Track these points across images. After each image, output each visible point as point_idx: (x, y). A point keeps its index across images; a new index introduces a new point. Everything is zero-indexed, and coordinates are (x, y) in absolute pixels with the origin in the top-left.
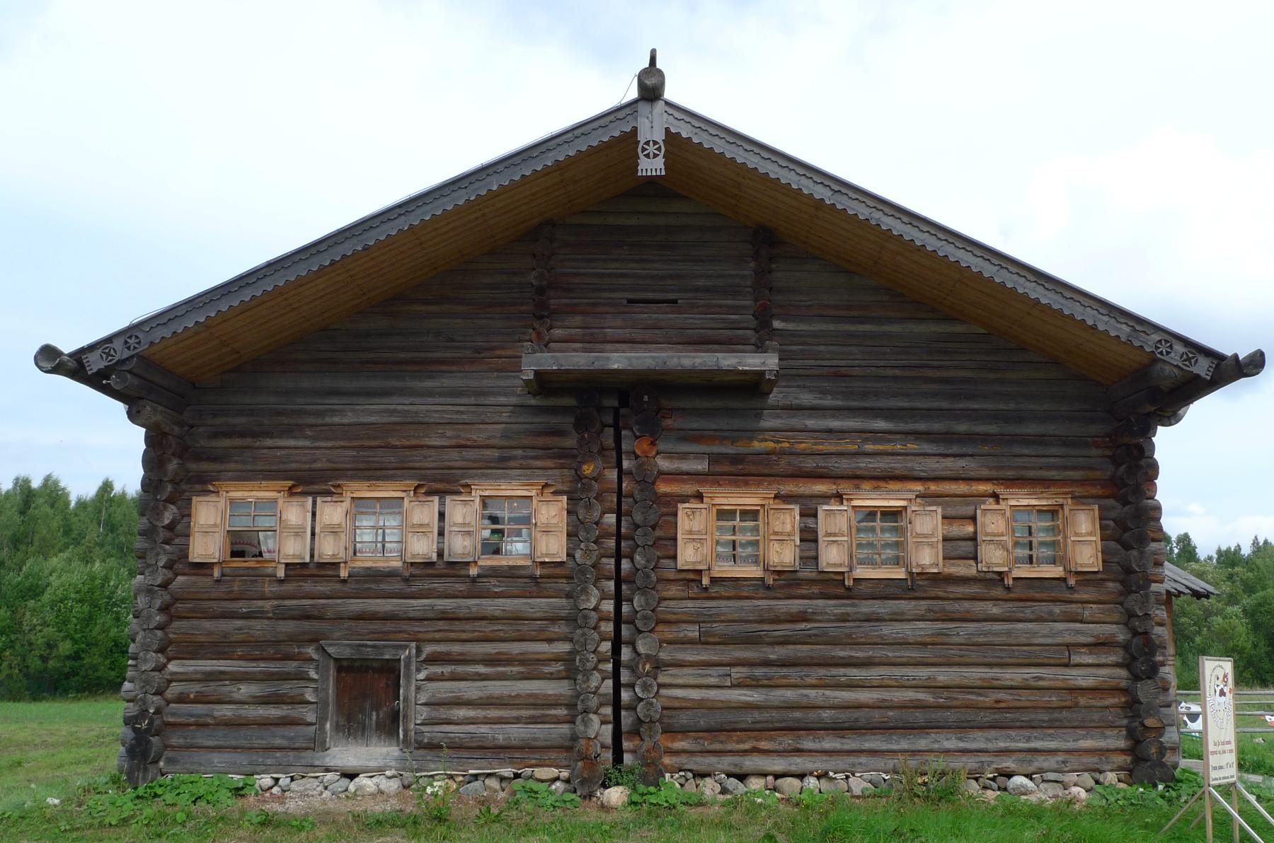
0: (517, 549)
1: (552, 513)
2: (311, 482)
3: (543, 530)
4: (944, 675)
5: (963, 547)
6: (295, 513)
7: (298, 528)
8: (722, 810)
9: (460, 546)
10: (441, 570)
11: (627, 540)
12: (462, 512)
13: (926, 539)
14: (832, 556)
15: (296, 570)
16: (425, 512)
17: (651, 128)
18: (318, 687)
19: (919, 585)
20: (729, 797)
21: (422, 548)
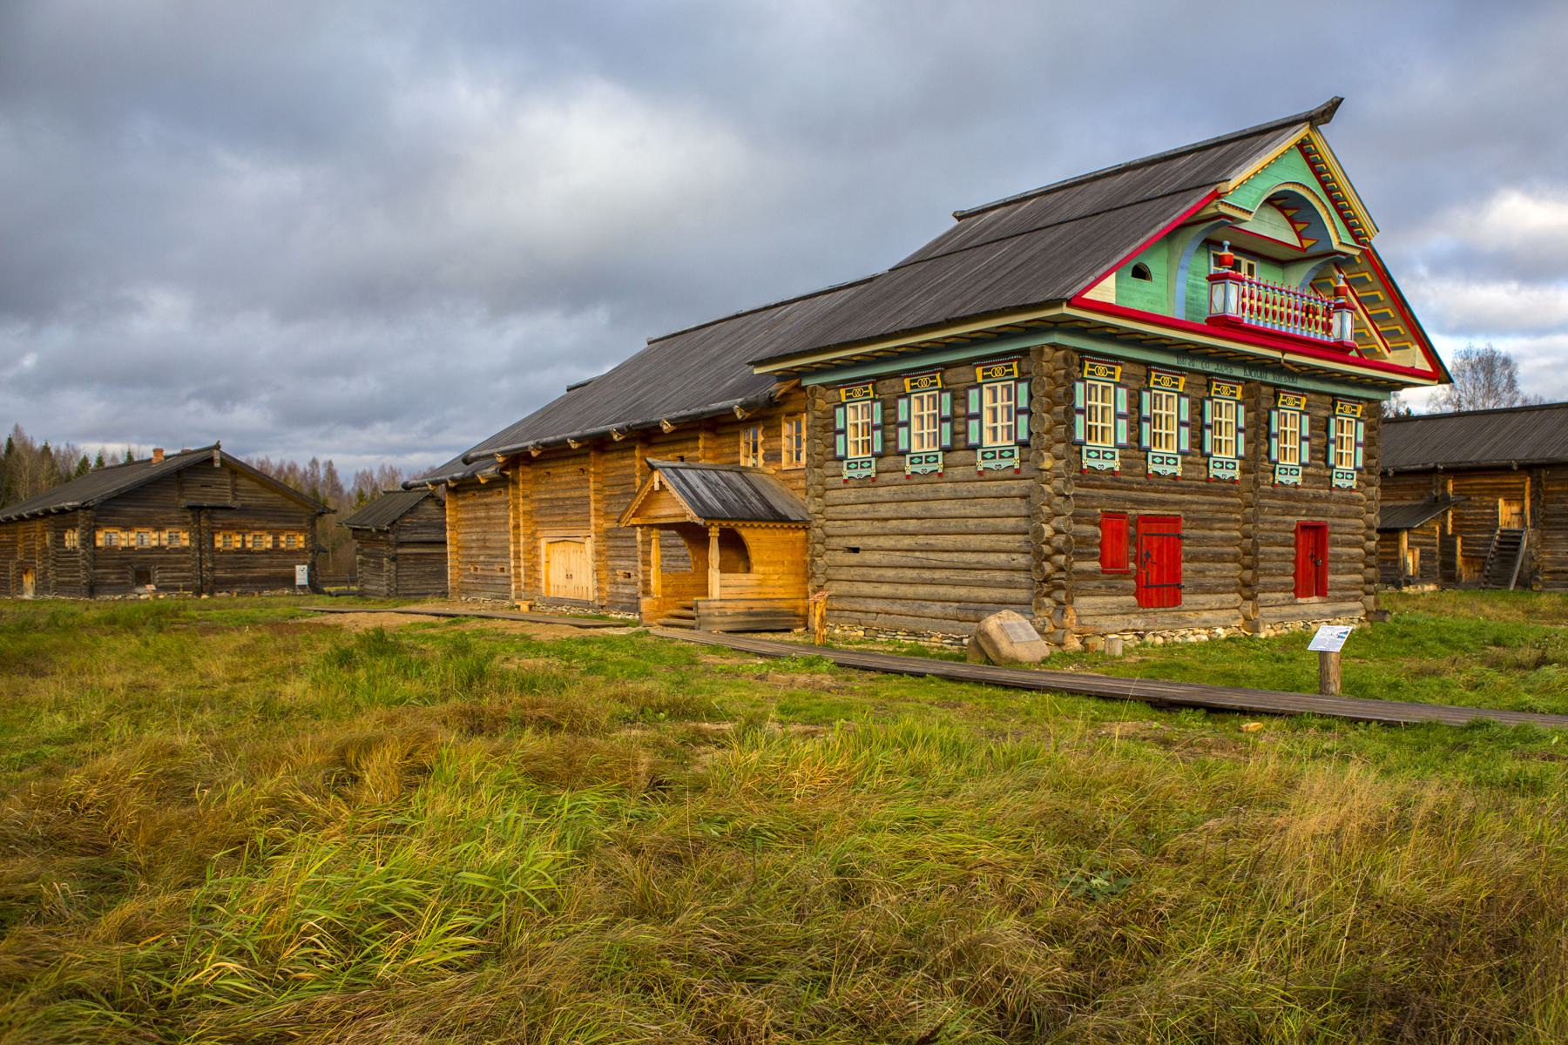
0: (177, 545)
1: (186, 535)
2: (126, 528)
3: (184, 539)
4: (1207, 533)
5: (276, 539)
6: (123, 535)
7: (125, 539)
8: (144, 631)
9: (165, 543)
10: (160, 548)
11: (203, 542)
12: (165, 535)
13: (267, 542)
14: (249, 545)
15: (124, 548)
16: (155, 535)
17: (217, 456)
18: (131, 575)
19: (267, 551)
20: (650, 460)
21: (155, 543)
